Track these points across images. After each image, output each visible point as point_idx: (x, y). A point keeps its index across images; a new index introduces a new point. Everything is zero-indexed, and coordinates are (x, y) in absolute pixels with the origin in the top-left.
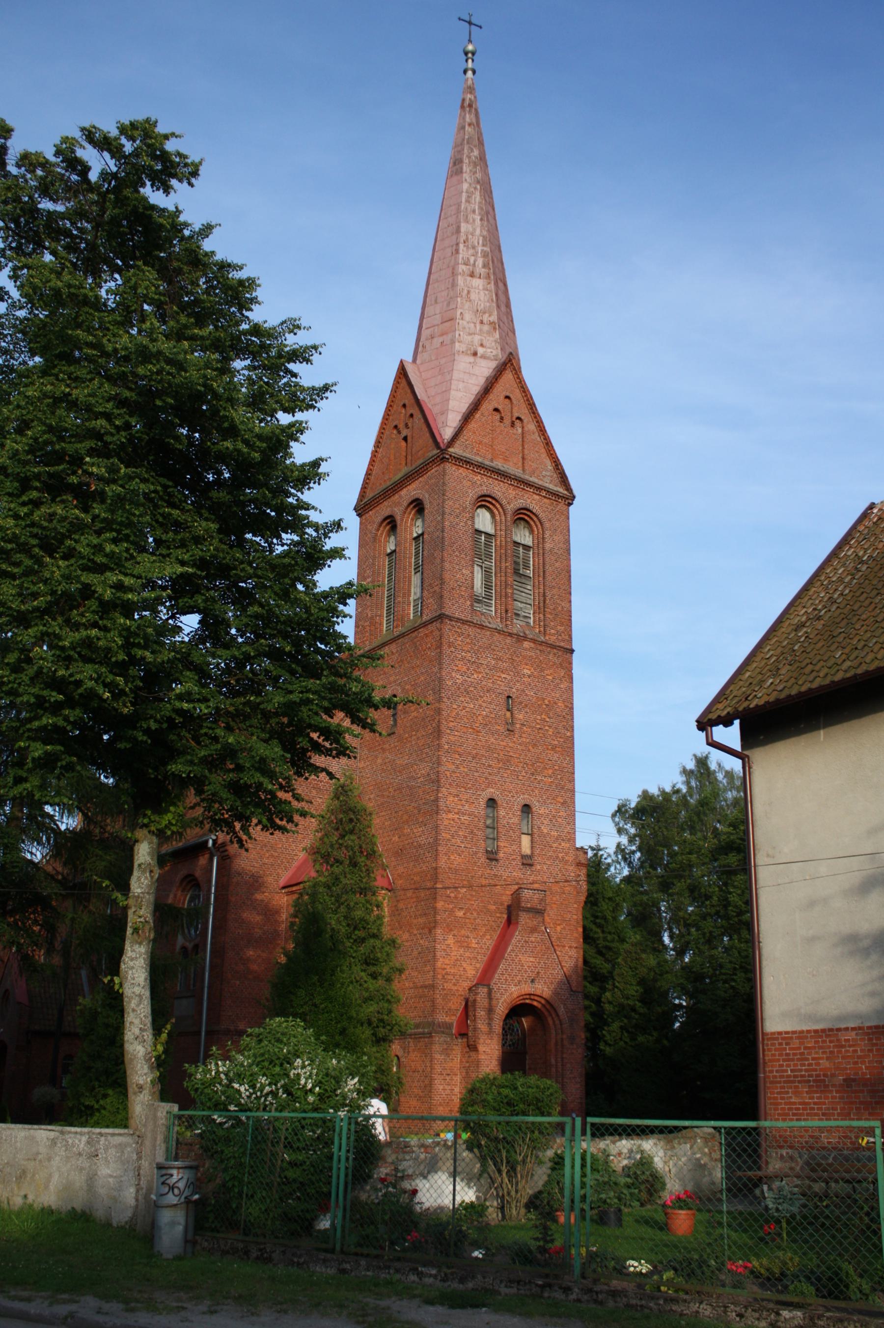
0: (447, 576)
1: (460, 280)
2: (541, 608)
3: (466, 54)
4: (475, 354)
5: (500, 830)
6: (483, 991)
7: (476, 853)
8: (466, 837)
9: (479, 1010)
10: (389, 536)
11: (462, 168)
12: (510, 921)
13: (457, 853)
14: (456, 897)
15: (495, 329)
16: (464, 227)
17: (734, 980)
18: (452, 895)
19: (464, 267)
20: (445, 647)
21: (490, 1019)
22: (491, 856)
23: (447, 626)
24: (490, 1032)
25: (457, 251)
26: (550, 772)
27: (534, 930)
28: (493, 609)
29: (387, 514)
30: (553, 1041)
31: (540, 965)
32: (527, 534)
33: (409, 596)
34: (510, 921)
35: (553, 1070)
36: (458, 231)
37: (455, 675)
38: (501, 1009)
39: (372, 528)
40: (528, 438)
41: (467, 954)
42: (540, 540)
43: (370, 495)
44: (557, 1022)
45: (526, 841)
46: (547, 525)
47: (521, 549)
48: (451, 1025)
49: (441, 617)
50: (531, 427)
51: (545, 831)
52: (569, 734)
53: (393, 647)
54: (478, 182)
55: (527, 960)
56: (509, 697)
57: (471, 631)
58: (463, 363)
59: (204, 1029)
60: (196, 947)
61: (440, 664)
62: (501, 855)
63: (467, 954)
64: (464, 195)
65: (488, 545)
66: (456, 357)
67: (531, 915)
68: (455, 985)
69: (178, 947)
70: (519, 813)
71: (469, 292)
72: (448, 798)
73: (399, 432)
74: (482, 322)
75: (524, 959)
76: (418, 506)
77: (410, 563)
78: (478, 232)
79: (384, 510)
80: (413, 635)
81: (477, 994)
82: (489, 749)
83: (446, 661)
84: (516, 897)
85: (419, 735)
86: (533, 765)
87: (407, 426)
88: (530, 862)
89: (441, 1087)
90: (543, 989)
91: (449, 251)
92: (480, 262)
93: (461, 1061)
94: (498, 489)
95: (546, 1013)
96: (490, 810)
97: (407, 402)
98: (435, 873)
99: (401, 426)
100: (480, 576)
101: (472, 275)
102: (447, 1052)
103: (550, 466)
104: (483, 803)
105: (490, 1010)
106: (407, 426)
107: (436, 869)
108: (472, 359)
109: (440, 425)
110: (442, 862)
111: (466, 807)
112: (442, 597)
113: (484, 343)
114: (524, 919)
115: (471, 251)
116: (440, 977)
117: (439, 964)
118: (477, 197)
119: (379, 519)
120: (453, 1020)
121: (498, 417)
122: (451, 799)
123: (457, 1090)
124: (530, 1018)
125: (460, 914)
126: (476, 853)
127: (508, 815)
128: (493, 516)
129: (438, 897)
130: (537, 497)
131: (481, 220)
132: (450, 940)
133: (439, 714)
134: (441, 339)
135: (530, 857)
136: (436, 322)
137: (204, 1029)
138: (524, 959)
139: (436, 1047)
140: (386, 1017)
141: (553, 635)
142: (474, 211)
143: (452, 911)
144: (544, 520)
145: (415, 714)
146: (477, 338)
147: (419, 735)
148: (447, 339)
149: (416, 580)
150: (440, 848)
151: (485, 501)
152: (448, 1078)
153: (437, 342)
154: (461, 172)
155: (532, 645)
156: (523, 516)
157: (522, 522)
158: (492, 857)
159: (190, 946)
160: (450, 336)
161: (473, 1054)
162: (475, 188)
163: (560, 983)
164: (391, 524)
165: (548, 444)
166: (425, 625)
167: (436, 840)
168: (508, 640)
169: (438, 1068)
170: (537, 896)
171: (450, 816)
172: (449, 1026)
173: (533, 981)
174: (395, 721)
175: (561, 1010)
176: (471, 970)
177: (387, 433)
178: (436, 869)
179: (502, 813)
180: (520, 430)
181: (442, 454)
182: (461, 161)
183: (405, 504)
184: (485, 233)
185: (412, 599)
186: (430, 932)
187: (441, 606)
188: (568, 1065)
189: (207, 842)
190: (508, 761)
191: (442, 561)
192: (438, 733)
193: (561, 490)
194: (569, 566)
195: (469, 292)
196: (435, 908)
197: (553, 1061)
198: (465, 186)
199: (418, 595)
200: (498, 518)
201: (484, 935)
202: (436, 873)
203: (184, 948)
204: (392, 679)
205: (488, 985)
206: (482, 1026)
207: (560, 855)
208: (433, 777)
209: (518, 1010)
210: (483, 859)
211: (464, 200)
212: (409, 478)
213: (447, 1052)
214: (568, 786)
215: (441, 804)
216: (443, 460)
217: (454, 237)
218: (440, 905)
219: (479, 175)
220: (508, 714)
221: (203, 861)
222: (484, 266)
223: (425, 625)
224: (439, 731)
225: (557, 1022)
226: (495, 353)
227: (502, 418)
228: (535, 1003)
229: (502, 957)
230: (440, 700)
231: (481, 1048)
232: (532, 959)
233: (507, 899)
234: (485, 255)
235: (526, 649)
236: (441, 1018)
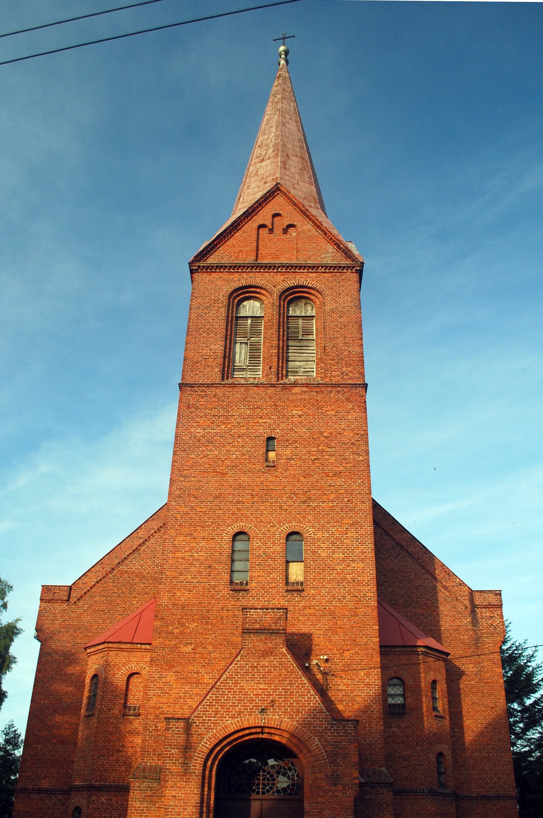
14: (182, 633)
18: (176, 631)
155: (305, 389)
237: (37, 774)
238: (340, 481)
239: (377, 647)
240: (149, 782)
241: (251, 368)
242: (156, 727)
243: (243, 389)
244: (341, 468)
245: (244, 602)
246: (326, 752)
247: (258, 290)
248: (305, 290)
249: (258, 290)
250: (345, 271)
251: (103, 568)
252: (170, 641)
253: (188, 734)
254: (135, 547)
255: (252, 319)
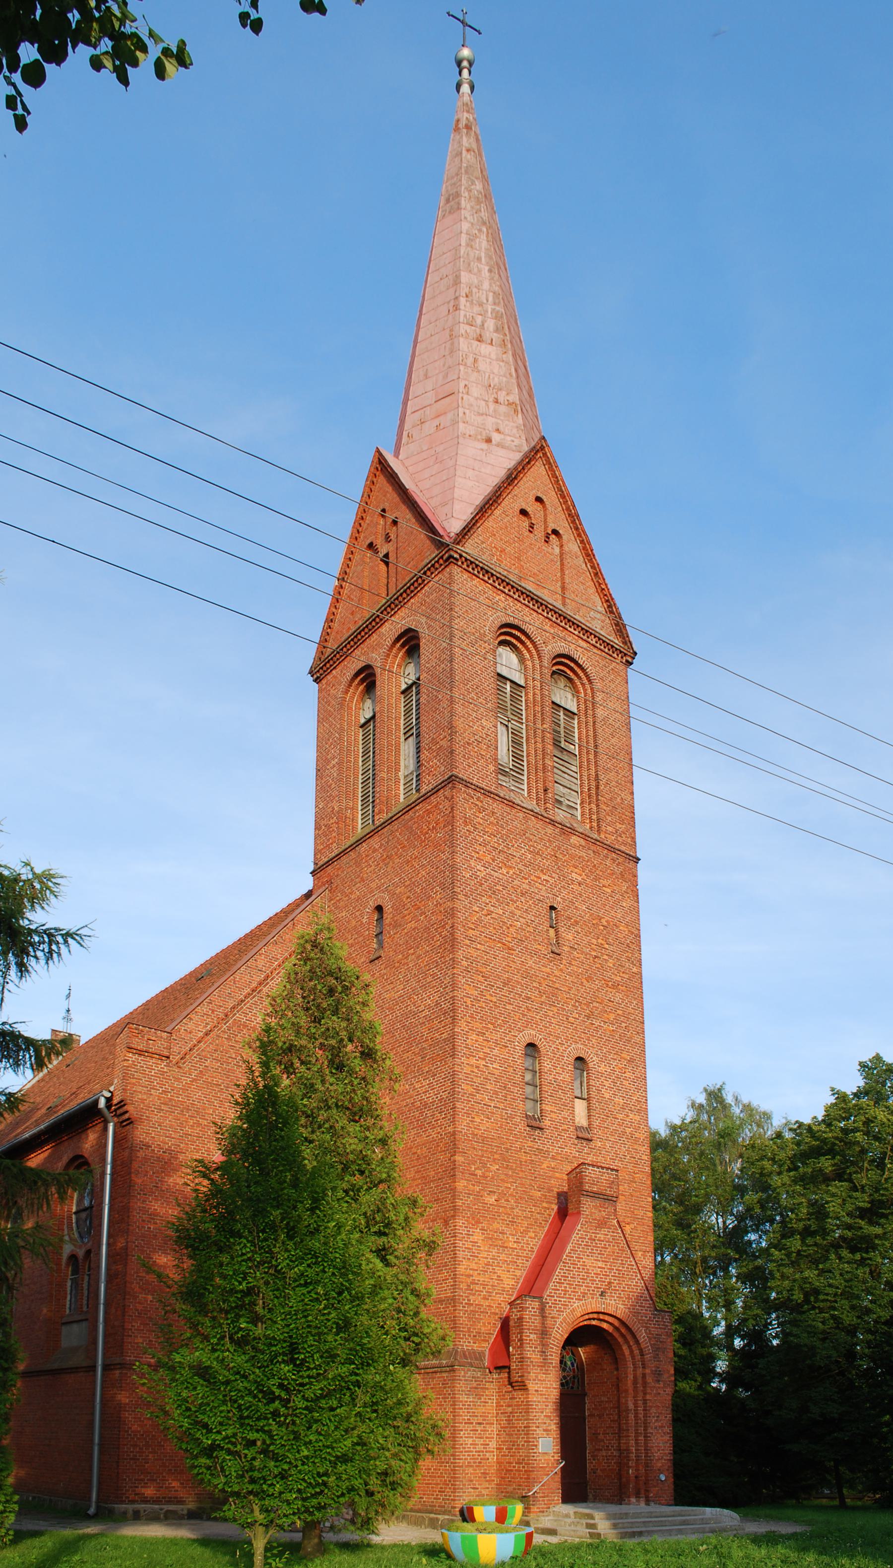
0: (459, 724)
1: (463, 344)
2: (593, 794)
3: (459, 63)
4: (489, 440)
5: (545, 1088)
6: (532, 1305)
7: (511, 1117)
8: (496, 1093)
9: (526, 1333)
10: (362, 700)
11: (459, 204)
12: (565, 1210)
13: (485, 1110)
14: (484, 1177)
15: (516, 411)
16: (465, 277)
17: (834, 1309)
18: (479, 1172)
19: (468, 328)
20: (459, 823)
21: (544, 1345)
22: (534, 1123)
23: (461, 795)
24: (544, 1364)
25: (457, 308)
26: (612, 1017)
27: (602, 1224)
28: (525, 787)
29: (360, 665)
30: (631, 1377)
31: (608, 1274)
32: (570, 696)
33: (398, 770)
34: (565, 1210)
35: (632, 1416)
36: (457, 282)
37: (473, 865)
38: (560, 1332)
39: (338, 692)
40: (568, 561)
41: (503, 1257)
42: (590, 705)
43: (332, 645)
44: (636, 1352)
45: (580, 1107)
46: (598, 685)
47: (561, 714)
48: (482, 1354)
49: (451, 780)
50: (573, 546)
51: (607, 1096)
52: (635, 970)
53: (375, 842)
54: (484, 223)
55: (594, 1264)
56: (552, 908)
57: (497, 807)
58: (471, 449)
59: (100, 1362)
60: (88, 1252)
61: (452, 846)
62: (547, 1123)
63: (503, 1257)
64: (464, 237)
65: (515, 698)
66: (461, 440)
67: (598, 1202)
68: (485, 1298)
69: (65, 1256)
70: (571, 1067)
71: (475, 360)
72: (468, 1035)
73: (376, 551)
74: (496, 401)
75: (589, 1262)
76: (410, 642)
77: (397, 725)
78: (486, 285)
79: (353, 664)
80: (407, 817)
81: (523, 1309)
82: (527, 975)
83: (461, 843)
84: (576, 1176)
85: (419, 952)
86: (588, 1004)
87: (388, 539)
88: (589, 1136)
89: (470, 1441)
90: (617, 1305)
91: (444, 310)
92: (491, 324)
93: (498, 1405)
94: (531, 621)
95: (620, 1340)
96: (528, 1063)
97: (387, 506)
98: (452, 1144)
99: (379, 542)
100: (505, 739)
101: (480, 339)
102: (477, 1391)
103: (600, 607)
104: (520, 1049)
105: (544, 1333)
106: (388, 539)
107: (454, 1134)
108: (485, 446)
109: (443, 518)
110: (463, 1125)
111: (496, 1052)
112: (452, 752)
113: (501, 429)
114: (588, 1207)
115: (476, 309)
116: (463, 1286)
117: (461, 1269)
118: (483, 242)
119: (349, 674)
120: (485, 1348)
121: (526, 524)
122: (474, 1037)
123: (493, 1445)
124: (590, 1348)
125: (492, 1200)
126: (511, 1117)
127: (556, 1068)
128: (522, 660)
129: (459, 1175)
130: (584, 645)
131: (490, 271)
132: (478, 1236)
133: (453, 916)
134: (436, 422)
135: (589, 1128)
136: (429, 402)
137: (100, 1362)
138: (589, 1262)
139: (460, 1386)
140: (412, 1322)
141: (612, 834)
142: (479, 259)
143: (479, 1195)
144: (593, 676)
145: (413, 924)
146: (490, 422)
147: (419, 952)
148: (445, 420)
149: (407, 749)
150: (458, 1105)
151: (511, 635)
152: (479, 1428)
153: (430, 427)
154: (459, 208)
155: (583, 842)
156: (565, 667)
157: (562, 679)
158: (535, 1125)
159: (81, 1253)
160: (450, 416)
161: (518, 1394)
162: (480, 230)
163: (639, 1298)
164: (367, 679)
165: (597, 574)
166: (425, 798)
167: (453, 1092)
168: (550, 829)
169: (464, 1415)
170: (606, 1177)
171: (473, 1061)
172: (479, 1356)
173: (602, 1294)
174: (381, 945)
175: (642, 1336)
176: (511, 1279)
177: (357, 557)
178: (454, 1134)
179: (547, 1065)
180: (557, 550)
181: (446, 553)
182: (458, 195)
183: (389, 642)
184: (497, 289)
185: (401, 774)
186: (446, 1223)
187: (452, 765)
188: (653, 1410)
189: (96, 1102)
190: (554, 995)
191: (452, 701)
192: (452, 943)
193: (617, 642)
194: (629, 746)
195: (475, 360)
196: (454, 1190)
197: (631, 1406)
198: (465, 226)
199: (412, 767)
200: (529, 663)
201: (526, 1232)
202: (454, 1142)
203: (73, 1257)
204: (373, 885)
205: (541, 1297)
206: (532, 1354)
207: (628, 1130)
208: (445, 1006)
209: (582, 1335)
210: (522, 1126)
211: (463, 243)
212: (393, 605)
213: (477, 1391)
214: (637, 1039)
215: (459, 1042)
216: (450, 561)
217: (452, 291)
218: (461, 1185)
219: (484, 214)
220: (552, 931)
221: (92, 1136)
222: (497, 330)
223: (425, 798)
224: (454, 939)
225: (636, 1352)
226: (517, 442)
227: (532, 526)
228: (605, 1326)
229: (559, 1258)
230: (453, 897)
231: (532, 1386)
232: (600, 1264)
233: (560, 1182)
234: (497, 317)
235: (574, 846)
236: (467, 1344)
237: (150, 1341)
238: (618, 997)
239: (650, 1223)
240: (474, 1371)
241: (514, 774)
242: (469, 1300)
243: (521, 815)
244: (619, 979)
245: (538, 1145)
246: (651, 1345)
247: (523, 638)
248: (572, 665)
249: (523, 638)
250: (615, 655)
251: (213, 1011)
252: (474, 1185)
253: (543, 1317)
254: (254, 985)
255: (514, 686)
